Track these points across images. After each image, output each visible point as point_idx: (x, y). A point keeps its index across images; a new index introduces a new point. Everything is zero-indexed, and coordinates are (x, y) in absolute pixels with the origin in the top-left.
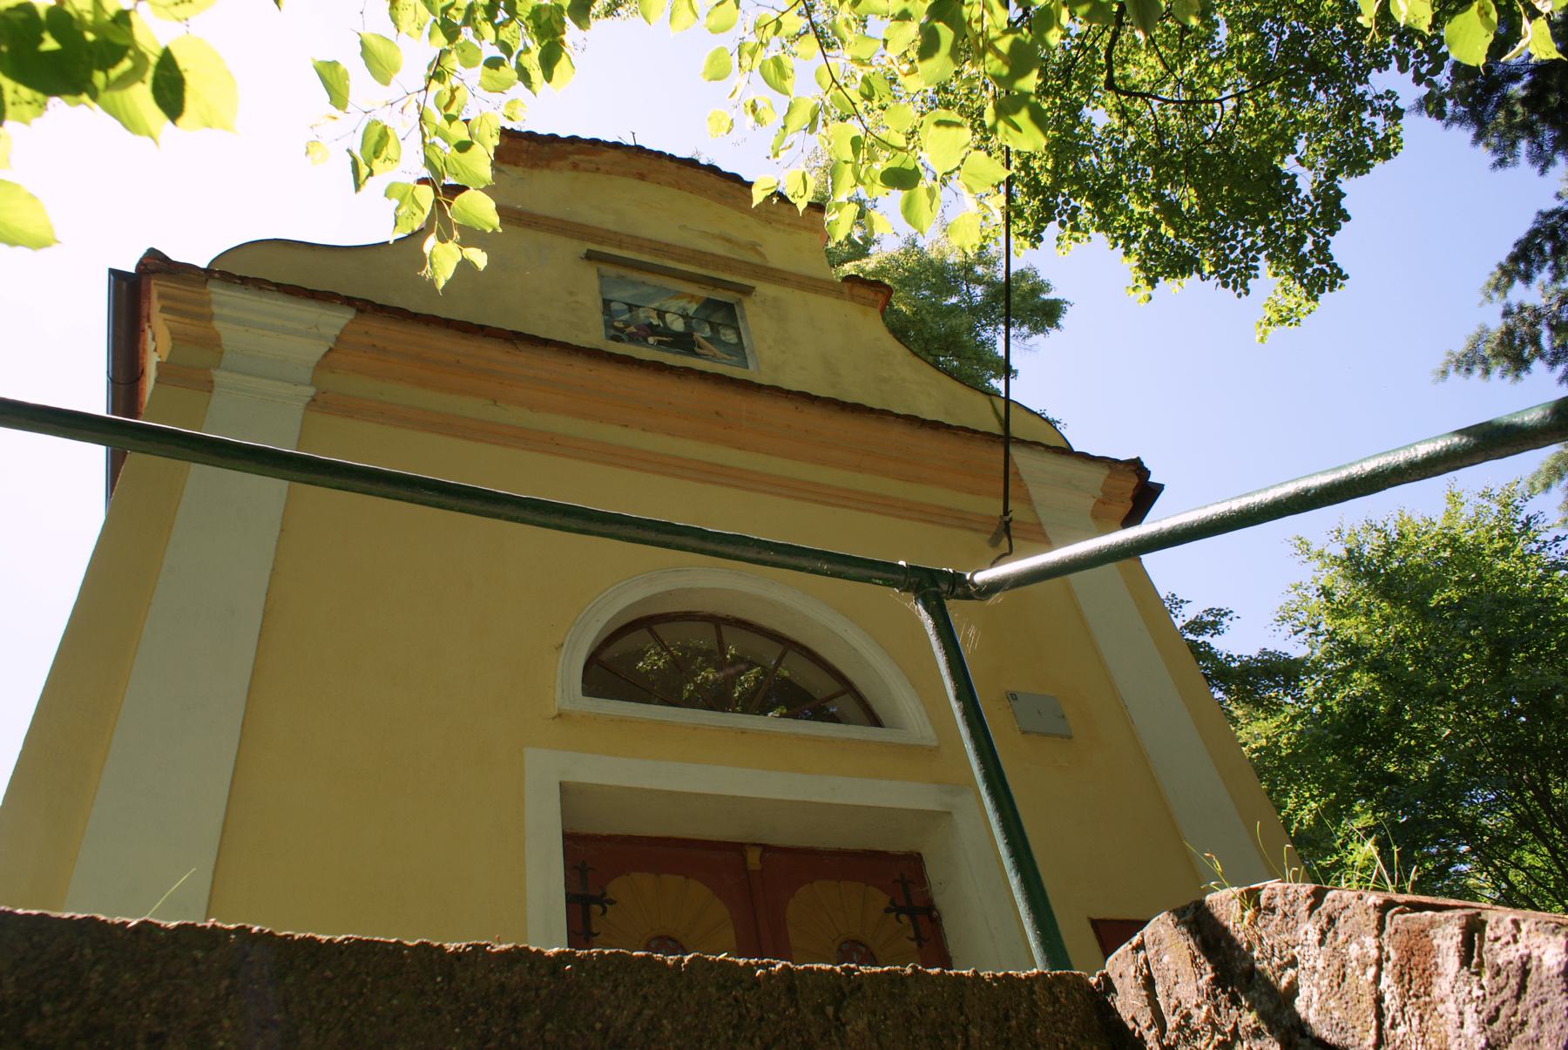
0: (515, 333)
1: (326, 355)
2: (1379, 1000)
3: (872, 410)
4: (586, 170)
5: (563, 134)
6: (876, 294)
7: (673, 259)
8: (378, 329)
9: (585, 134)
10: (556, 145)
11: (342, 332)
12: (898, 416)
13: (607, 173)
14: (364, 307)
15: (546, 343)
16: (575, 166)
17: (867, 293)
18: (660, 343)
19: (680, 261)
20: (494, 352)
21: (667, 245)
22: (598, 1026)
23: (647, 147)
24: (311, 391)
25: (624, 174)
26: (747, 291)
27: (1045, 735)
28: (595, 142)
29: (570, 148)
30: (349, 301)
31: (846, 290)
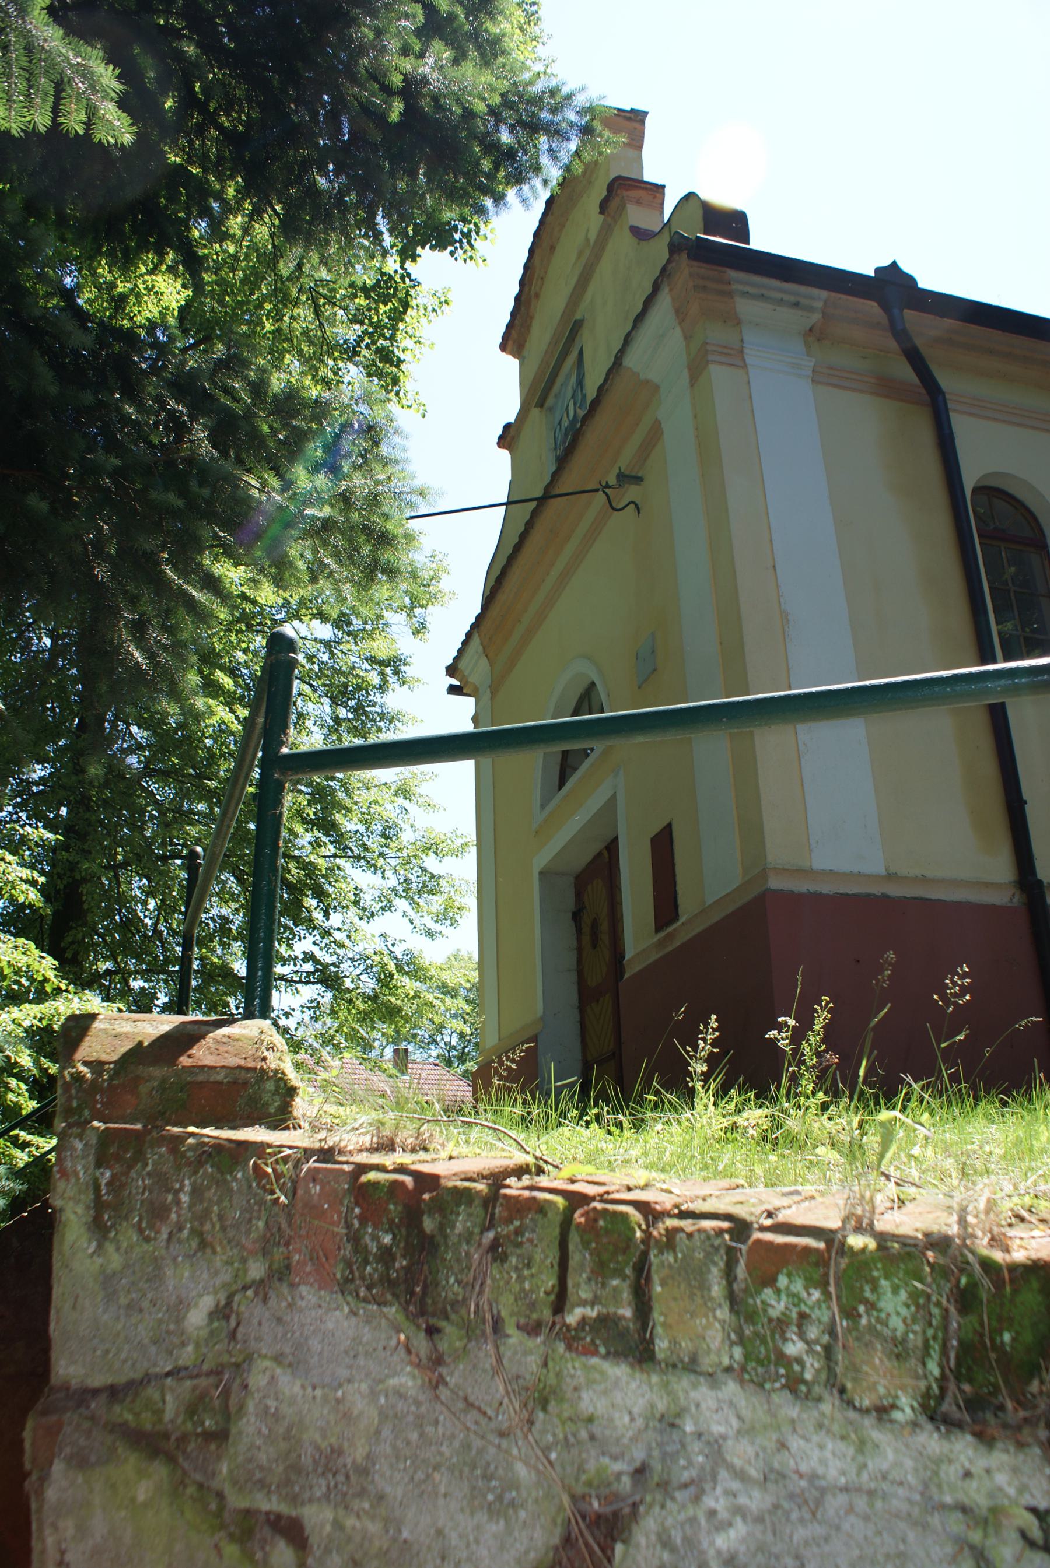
4: (541, 289)
13: (546, 272)
16: (537, 296)
28: (526, 267)
29: (526, 289)
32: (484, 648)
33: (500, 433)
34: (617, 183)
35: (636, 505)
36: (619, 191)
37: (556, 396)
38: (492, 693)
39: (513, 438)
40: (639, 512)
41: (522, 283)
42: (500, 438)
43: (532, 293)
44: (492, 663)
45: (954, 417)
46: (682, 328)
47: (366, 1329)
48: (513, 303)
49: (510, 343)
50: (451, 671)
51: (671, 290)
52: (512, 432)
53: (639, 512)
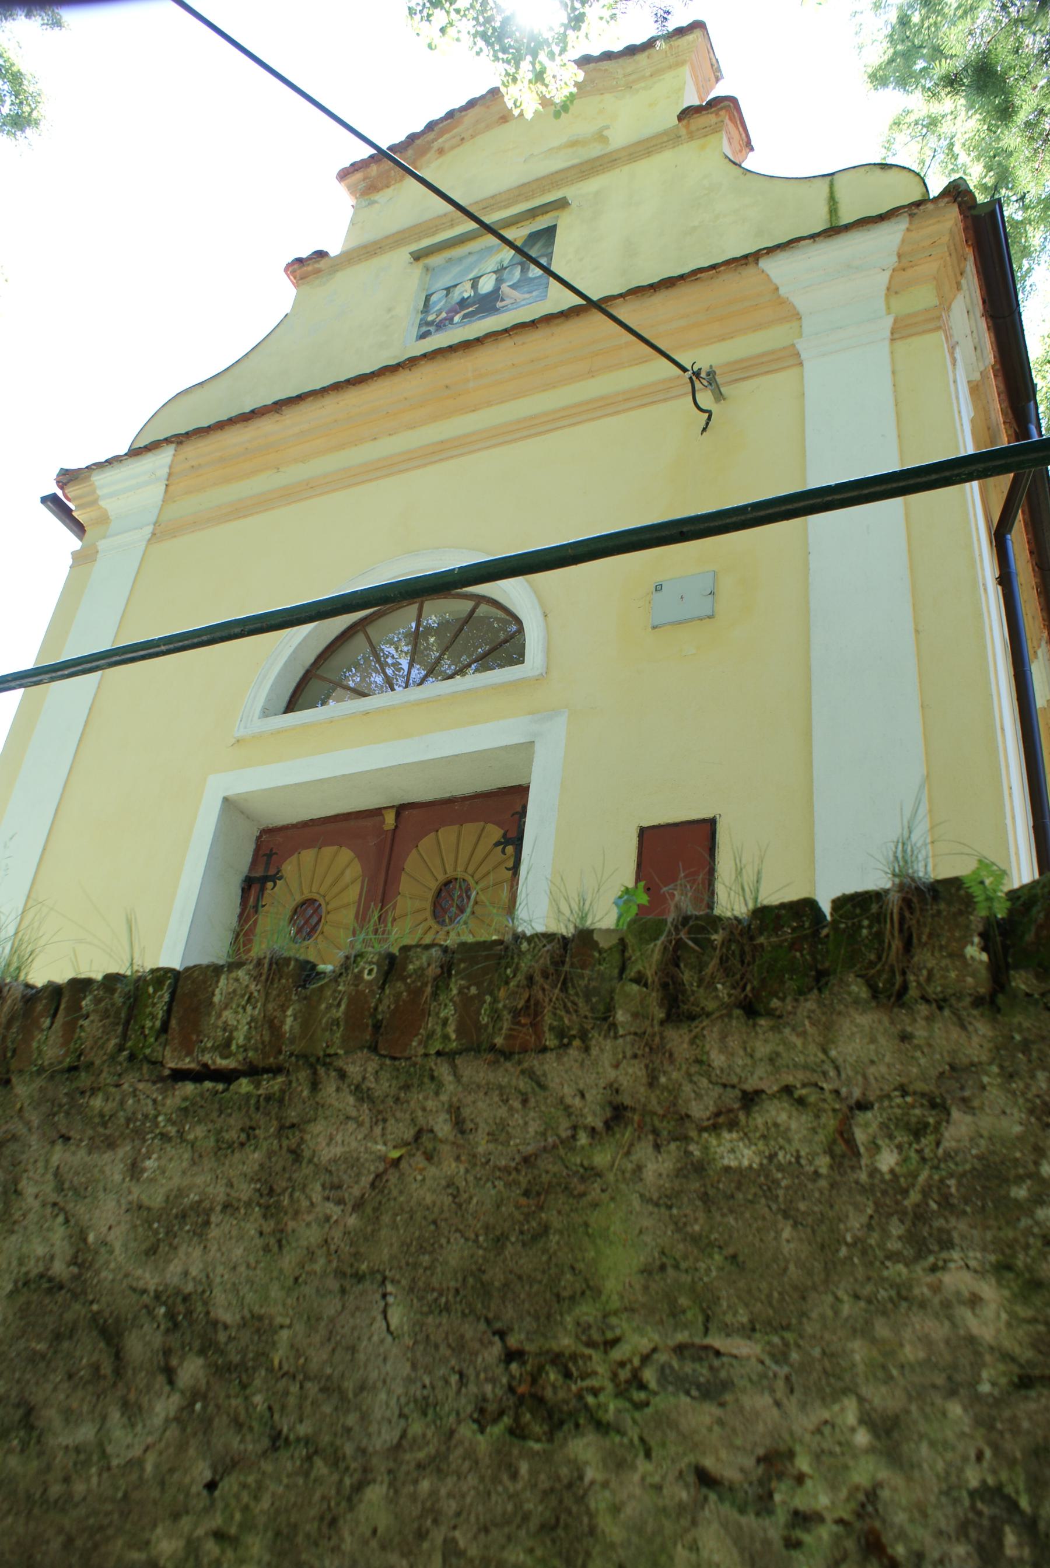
0: (276, 403)
1: (166, 491)
2: (342, 873)
3: (682, 277)
4: (453, 148)
5: (419, 128)
6: (717, 114)
7: (500, 209)
8: (194, 450)
9: (439, 113)
10: (418, 142)
11: (170, 467)
12: (621, 296)
13: (472, 137)
14: (179, 440)
15: (300, 398)
16: (441, 151)
17: (709, 119)
18: (465, 317)
19: (506, 207)
20: (267, 426)
21: (493, 197)
22: (1018, 1037)
23: (478, 95)
24: (889, 321)
25: (488, 127)
26: (562, 204)
27: (679, 623)
28: (451, 115)
29: (431, 136)
30: (167, 441)
31: (683, 132)
32: (170, 475)
33: (304, 254)
34: (727, 103)
35: (709, 418)
36: (722, 113)
37: (450, 260)
38: (154, 534)
39: (318, 271)
40: (704, 430)
41: (431, 126)
42: (299, 261)
43: (436, 145)
44: (168, 496)
45: (19, 692)
46: (892, 277)
47: (784, 1075)
48: (403, 138)
49: (359, 176)
50: (67, 477)
51: (908, 230)
52: (322, 264)
53: (704, 430)
